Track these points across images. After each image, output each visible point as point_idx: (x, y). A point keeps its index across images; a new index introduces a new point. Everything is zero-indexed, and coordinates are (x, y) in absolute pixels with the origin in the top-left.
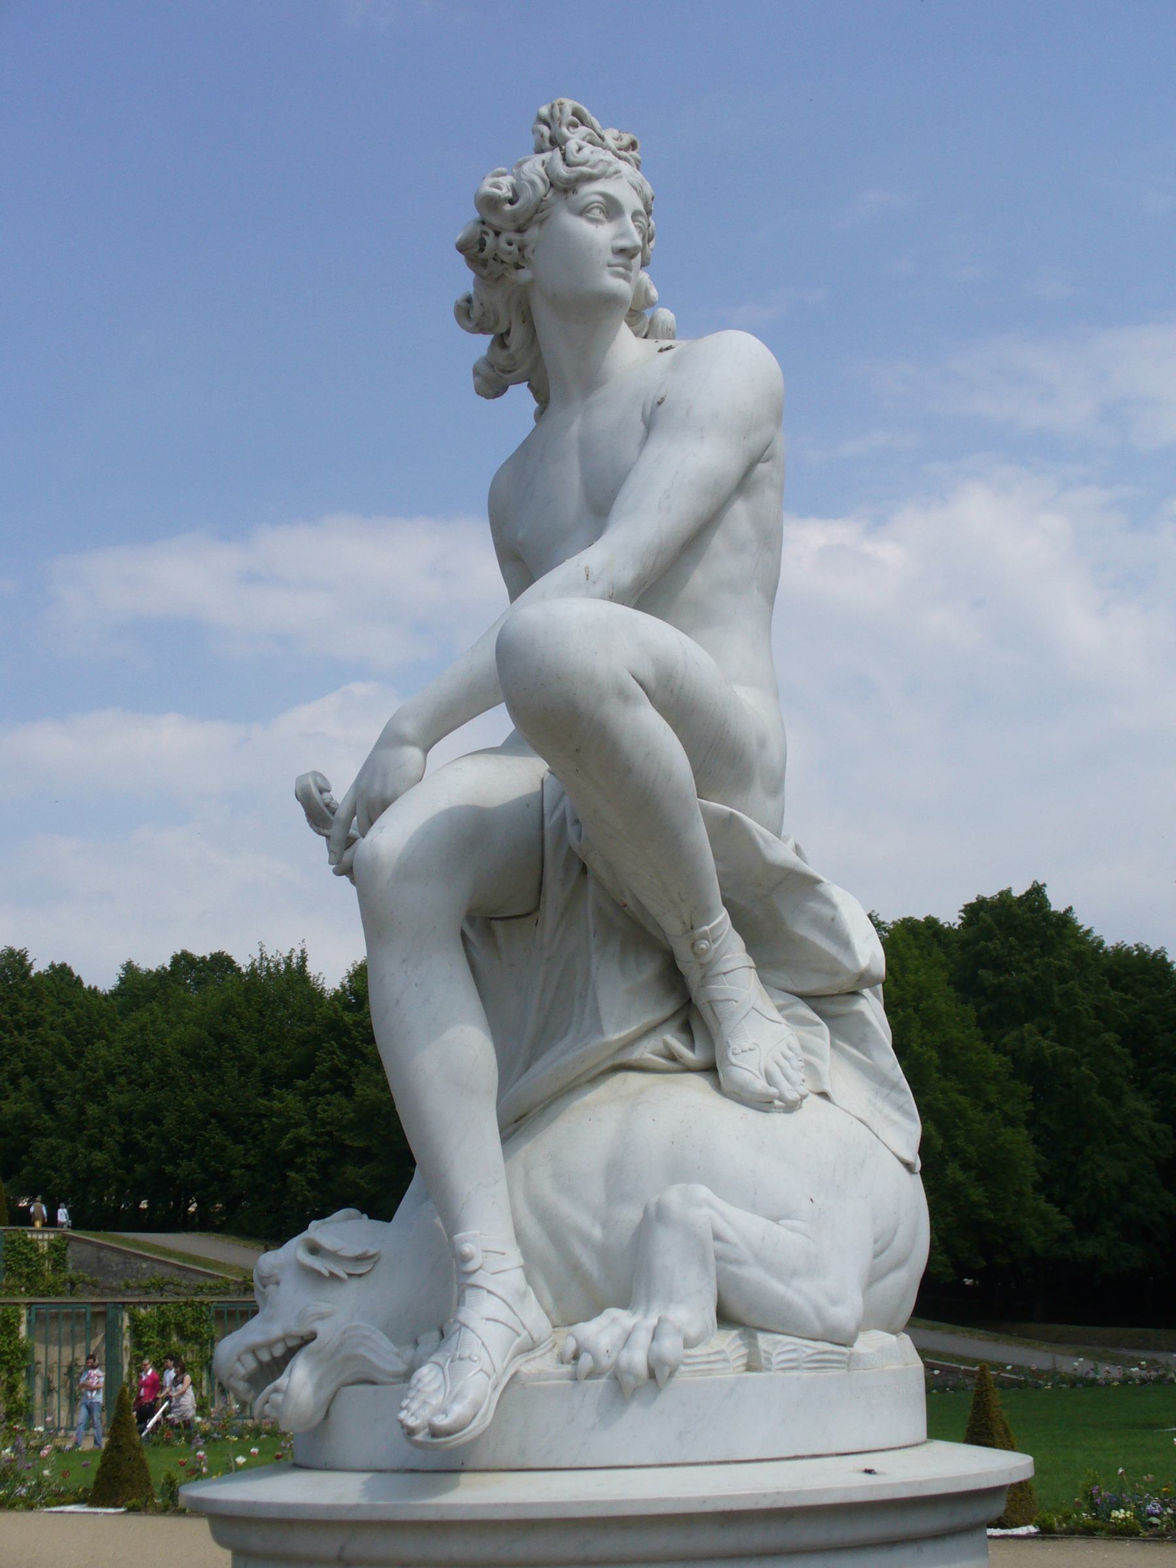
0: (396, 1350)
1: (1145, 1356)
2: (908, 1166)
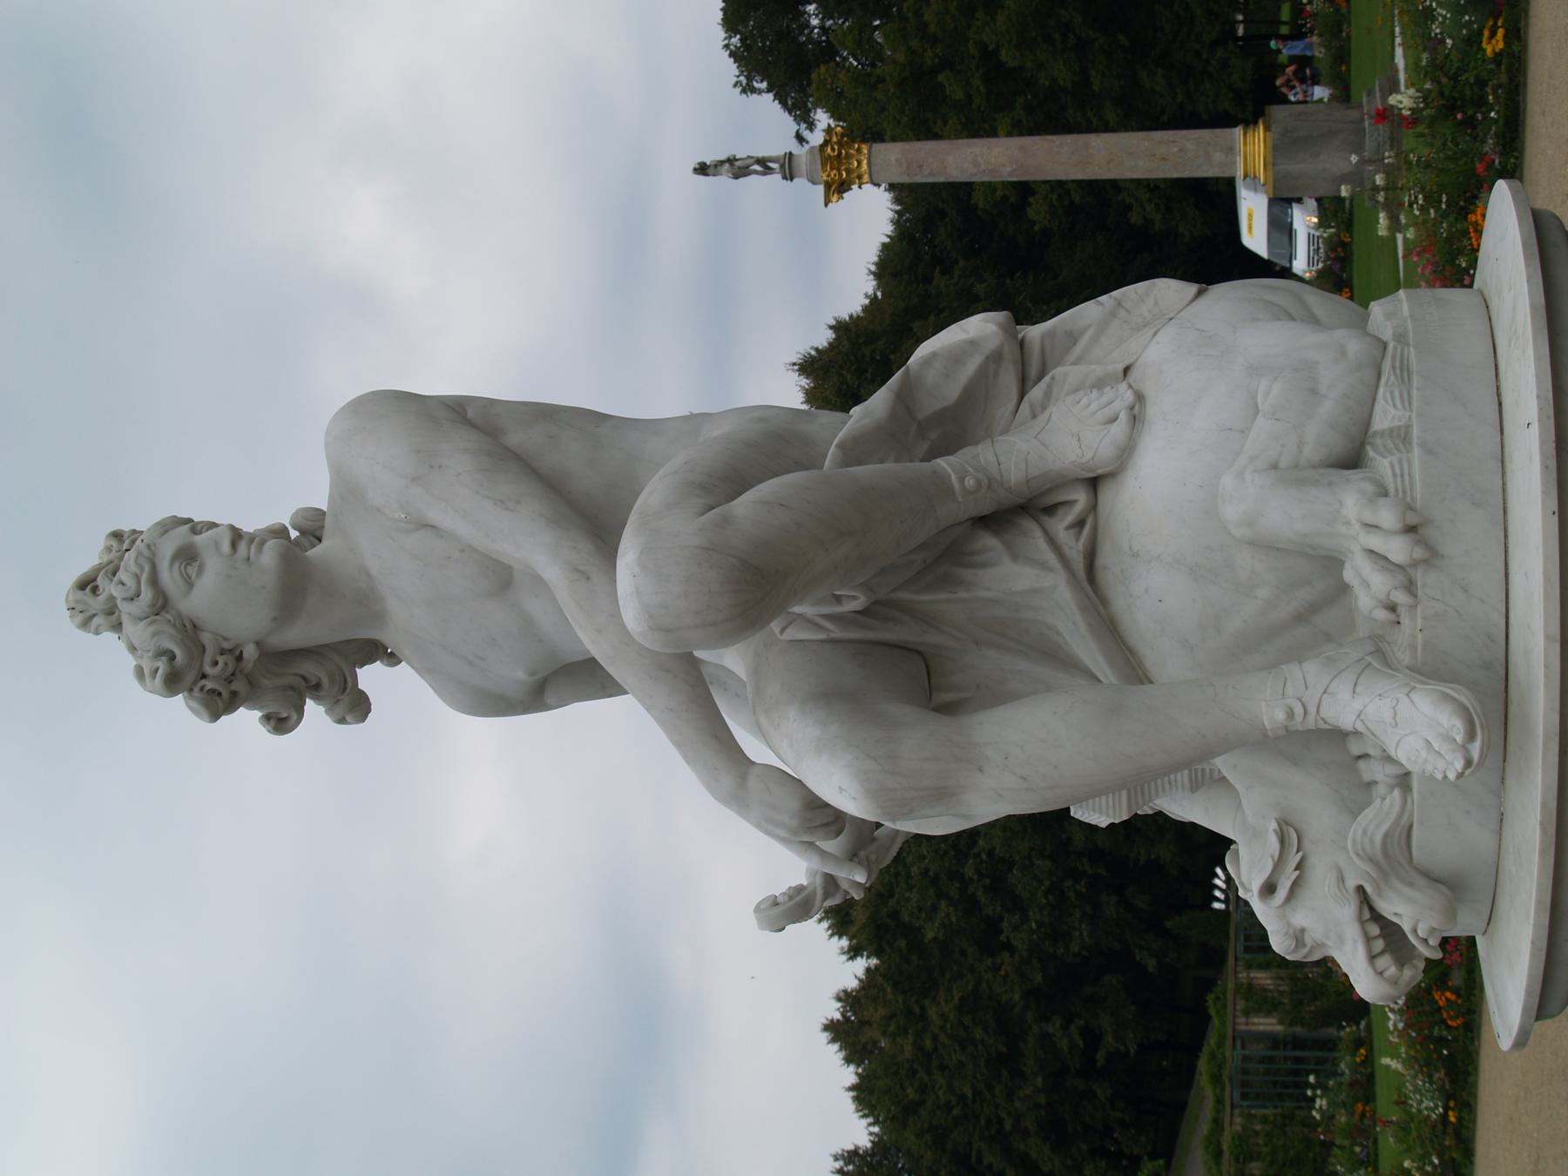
0: (1378, 801)
2: (1200, 293)
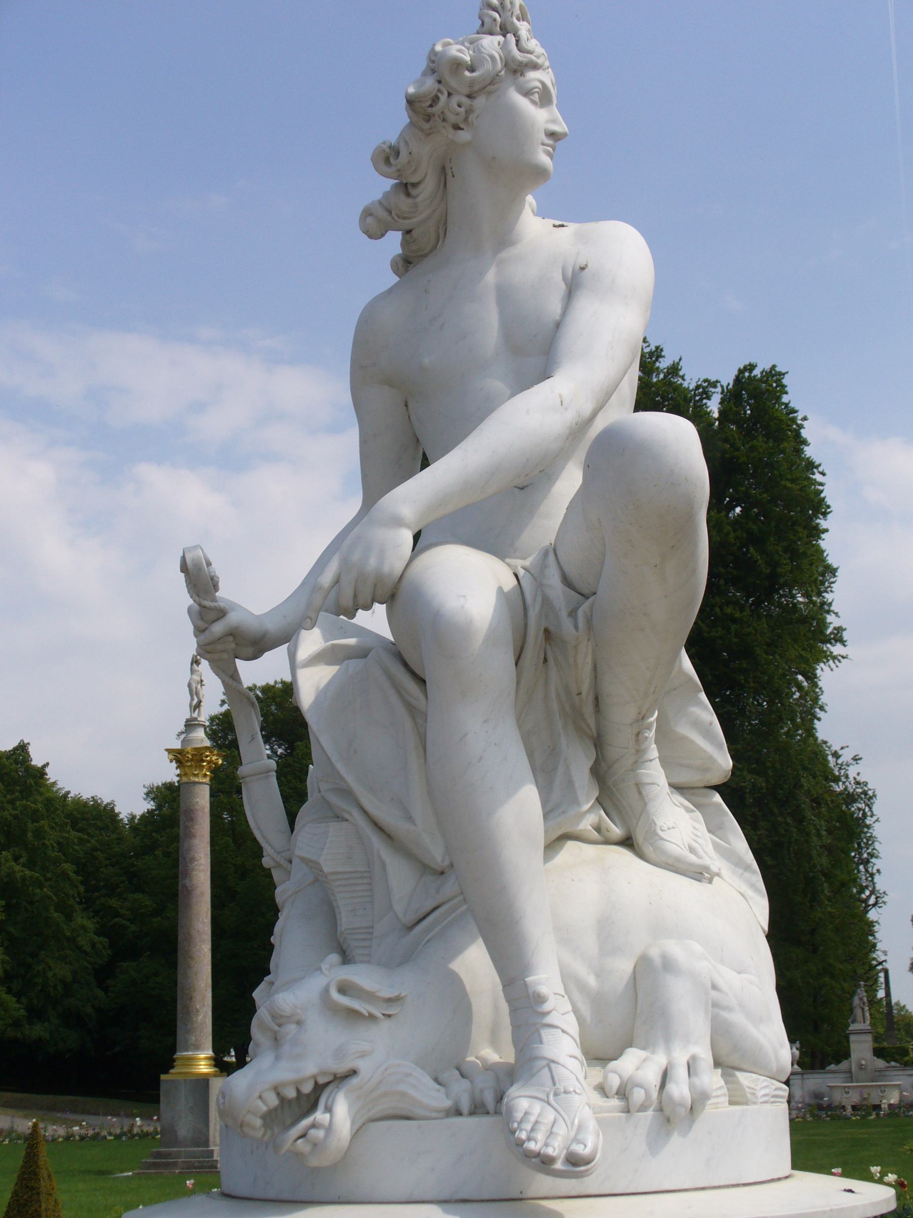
1: (93, 1120)
